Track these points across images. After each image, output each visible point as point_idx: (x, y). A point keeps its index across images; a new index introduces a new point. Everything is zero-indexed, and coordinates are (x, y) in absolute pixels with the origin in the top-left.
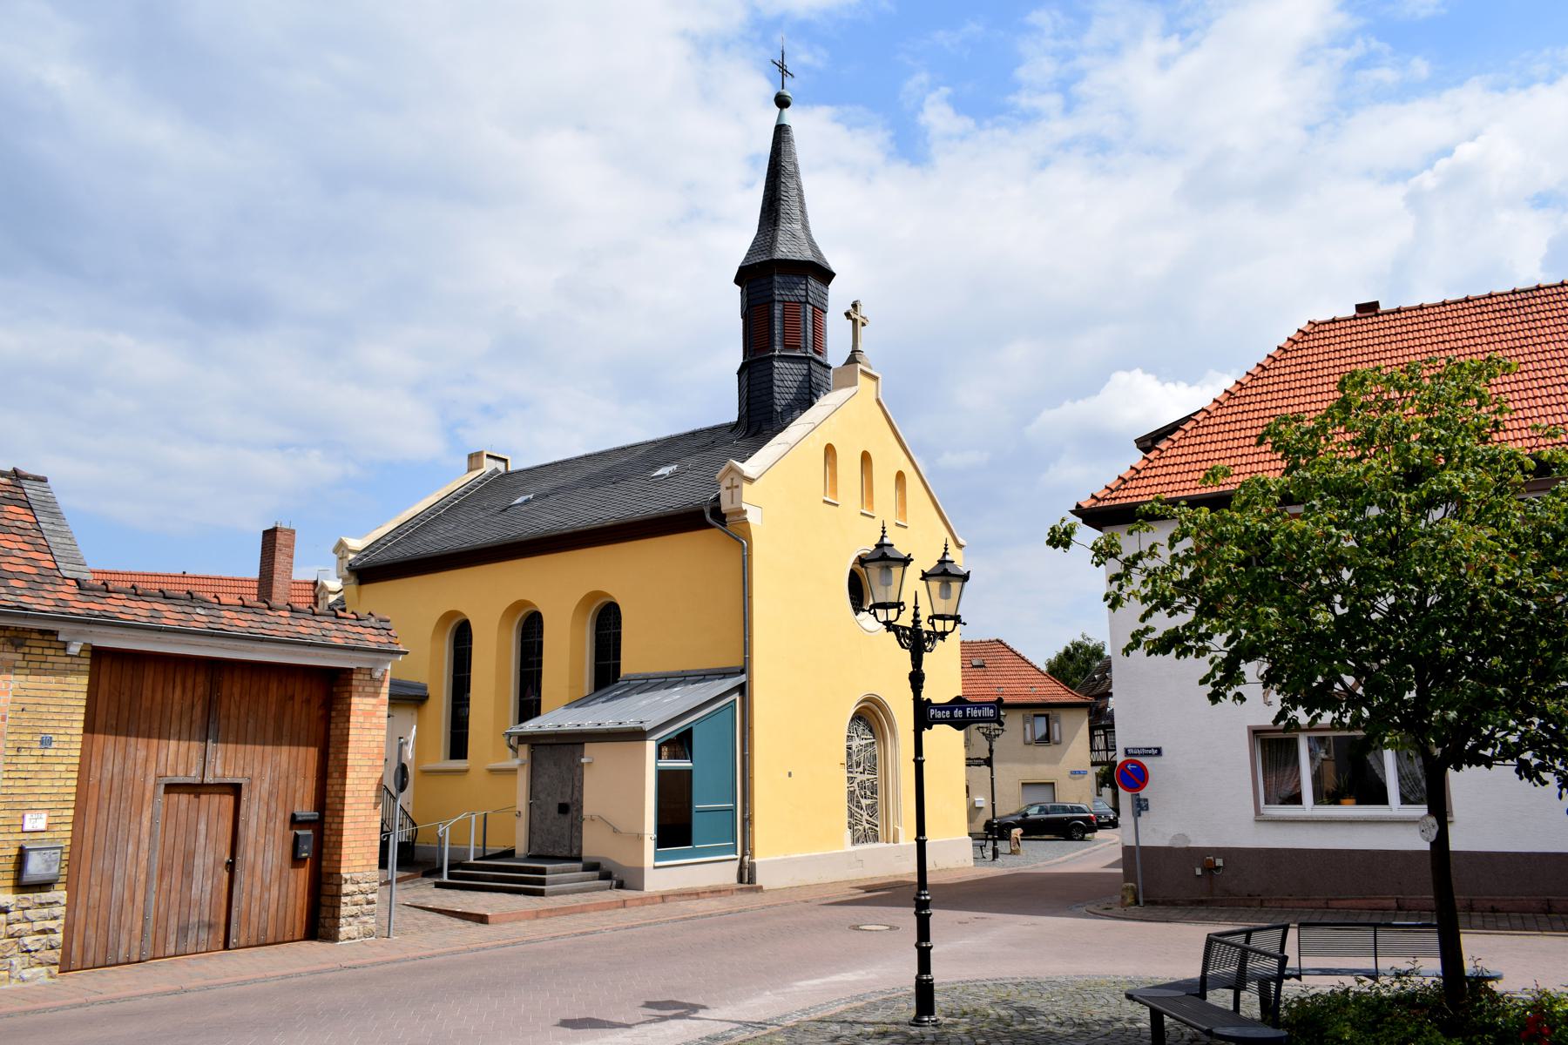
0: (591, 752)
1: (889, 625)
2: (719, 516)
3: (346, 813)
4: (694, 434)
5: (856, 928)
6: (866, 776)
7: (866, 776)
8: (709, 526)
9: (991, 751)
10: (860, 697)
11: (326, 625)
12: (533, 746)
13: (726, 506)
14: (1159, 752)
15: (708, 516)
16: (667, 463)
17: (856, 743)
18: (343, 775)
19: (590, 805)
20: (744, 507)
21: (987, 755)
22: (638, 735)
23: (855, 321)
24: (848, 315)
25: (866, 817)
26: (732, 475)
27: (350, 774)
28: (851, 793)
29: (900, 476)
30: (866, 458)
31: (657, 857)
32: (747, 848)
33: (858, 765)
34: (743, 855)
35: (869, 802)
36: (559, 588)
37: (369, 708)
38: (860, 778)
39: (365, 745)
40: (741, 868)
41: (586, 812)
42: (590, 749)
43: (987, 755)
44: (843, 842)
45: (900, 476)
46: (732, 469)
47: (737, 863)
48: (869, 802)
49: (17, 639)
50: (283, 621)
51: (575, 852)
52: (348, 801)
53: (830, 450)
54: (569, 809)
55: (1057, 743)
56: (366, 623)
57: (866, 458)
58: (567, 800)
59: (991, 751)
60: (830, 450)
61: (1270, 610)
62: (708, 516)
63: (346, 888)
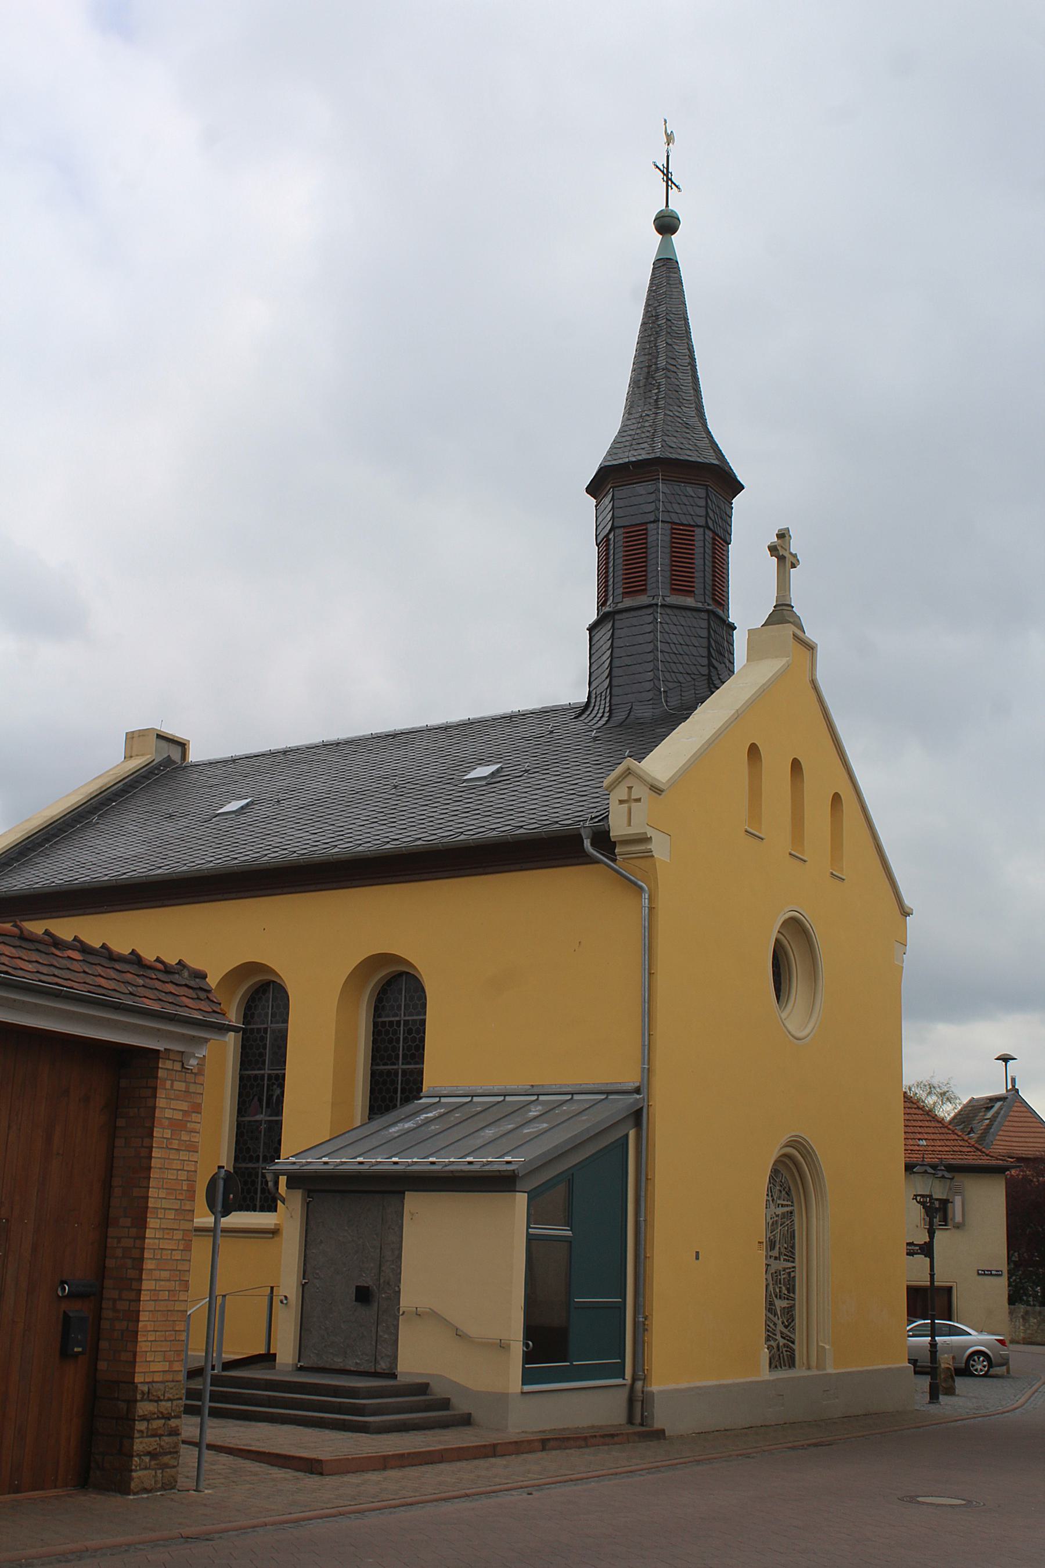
2: (604, 841)
3: (146, 1285)
4: (510, 718)
5: (912, 1499)
8: (595, 861)
10: (784, 1139)
11: (129, 977)
12: (309, 1193)
13: (618, 828)
15: (587, 843)
16: (482, 762)
18: (141, 1223)
19: (414, 1291)
22: (500, 1182)
24: (773, 549)
26: (630, 781)
27: (152, 1222)
29: (836, 798)
30: (796, 766)
31: (528, 1377)
32: (640, 1374)
34: (634, 1379)
35: (785, 1304)
36: (315, 950)
37: (179, 1116)
39: (171, 1175)
40: (631, 1401)
41: (407, 1300)
42: (414, 1203)
44: (765, 1374)
45: (836, 798)
46: (628, 772)
47: (626, 1391)
48: (785, 1304)
50: (76, 966)
51: (383, 1366)
52: (148, 1265)
53: (754, 751)
54: (374, 1296)
55: (958, 1227)
56: (176, 978)
57: (796, 766)
58: (366, 1281)
60: (754, 751)
61: (258, 1117)
62: (587, 843)
63: (144, 1408)
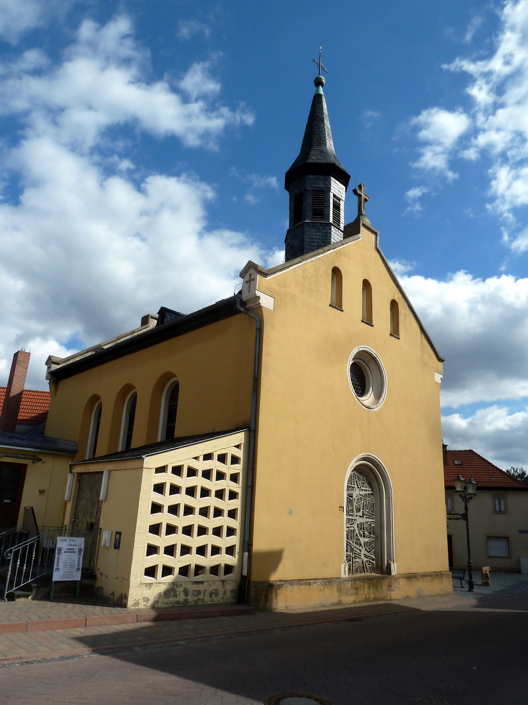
0: (465, 522)
1: (460, 495)
6: (363, 520)
7: (363, 520)
9: (466, 509)
14: (119, 533)
17: (356, 493)
20: (258, 293)
21: (463, 511)
23: (360, 196)
25: (364, 552)
28: (350, 534)
29: (394, 304)
30: (366, 284)
33: (358, 510)
38: (359, 520)
43: (463, 511)
48: (367, 540)
49: (524, 532)
57: (366, 284)
58: (93, 520)
59: (466, 509)
